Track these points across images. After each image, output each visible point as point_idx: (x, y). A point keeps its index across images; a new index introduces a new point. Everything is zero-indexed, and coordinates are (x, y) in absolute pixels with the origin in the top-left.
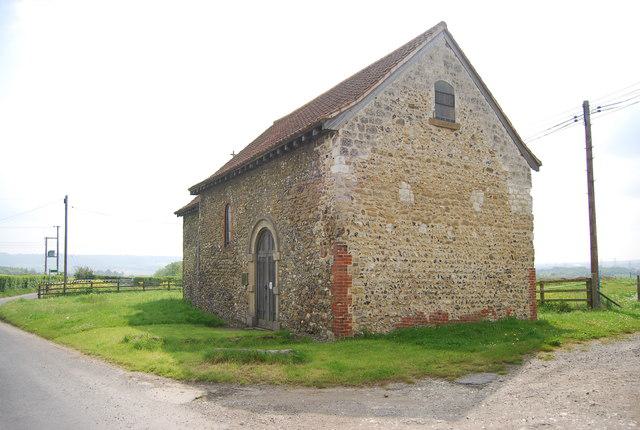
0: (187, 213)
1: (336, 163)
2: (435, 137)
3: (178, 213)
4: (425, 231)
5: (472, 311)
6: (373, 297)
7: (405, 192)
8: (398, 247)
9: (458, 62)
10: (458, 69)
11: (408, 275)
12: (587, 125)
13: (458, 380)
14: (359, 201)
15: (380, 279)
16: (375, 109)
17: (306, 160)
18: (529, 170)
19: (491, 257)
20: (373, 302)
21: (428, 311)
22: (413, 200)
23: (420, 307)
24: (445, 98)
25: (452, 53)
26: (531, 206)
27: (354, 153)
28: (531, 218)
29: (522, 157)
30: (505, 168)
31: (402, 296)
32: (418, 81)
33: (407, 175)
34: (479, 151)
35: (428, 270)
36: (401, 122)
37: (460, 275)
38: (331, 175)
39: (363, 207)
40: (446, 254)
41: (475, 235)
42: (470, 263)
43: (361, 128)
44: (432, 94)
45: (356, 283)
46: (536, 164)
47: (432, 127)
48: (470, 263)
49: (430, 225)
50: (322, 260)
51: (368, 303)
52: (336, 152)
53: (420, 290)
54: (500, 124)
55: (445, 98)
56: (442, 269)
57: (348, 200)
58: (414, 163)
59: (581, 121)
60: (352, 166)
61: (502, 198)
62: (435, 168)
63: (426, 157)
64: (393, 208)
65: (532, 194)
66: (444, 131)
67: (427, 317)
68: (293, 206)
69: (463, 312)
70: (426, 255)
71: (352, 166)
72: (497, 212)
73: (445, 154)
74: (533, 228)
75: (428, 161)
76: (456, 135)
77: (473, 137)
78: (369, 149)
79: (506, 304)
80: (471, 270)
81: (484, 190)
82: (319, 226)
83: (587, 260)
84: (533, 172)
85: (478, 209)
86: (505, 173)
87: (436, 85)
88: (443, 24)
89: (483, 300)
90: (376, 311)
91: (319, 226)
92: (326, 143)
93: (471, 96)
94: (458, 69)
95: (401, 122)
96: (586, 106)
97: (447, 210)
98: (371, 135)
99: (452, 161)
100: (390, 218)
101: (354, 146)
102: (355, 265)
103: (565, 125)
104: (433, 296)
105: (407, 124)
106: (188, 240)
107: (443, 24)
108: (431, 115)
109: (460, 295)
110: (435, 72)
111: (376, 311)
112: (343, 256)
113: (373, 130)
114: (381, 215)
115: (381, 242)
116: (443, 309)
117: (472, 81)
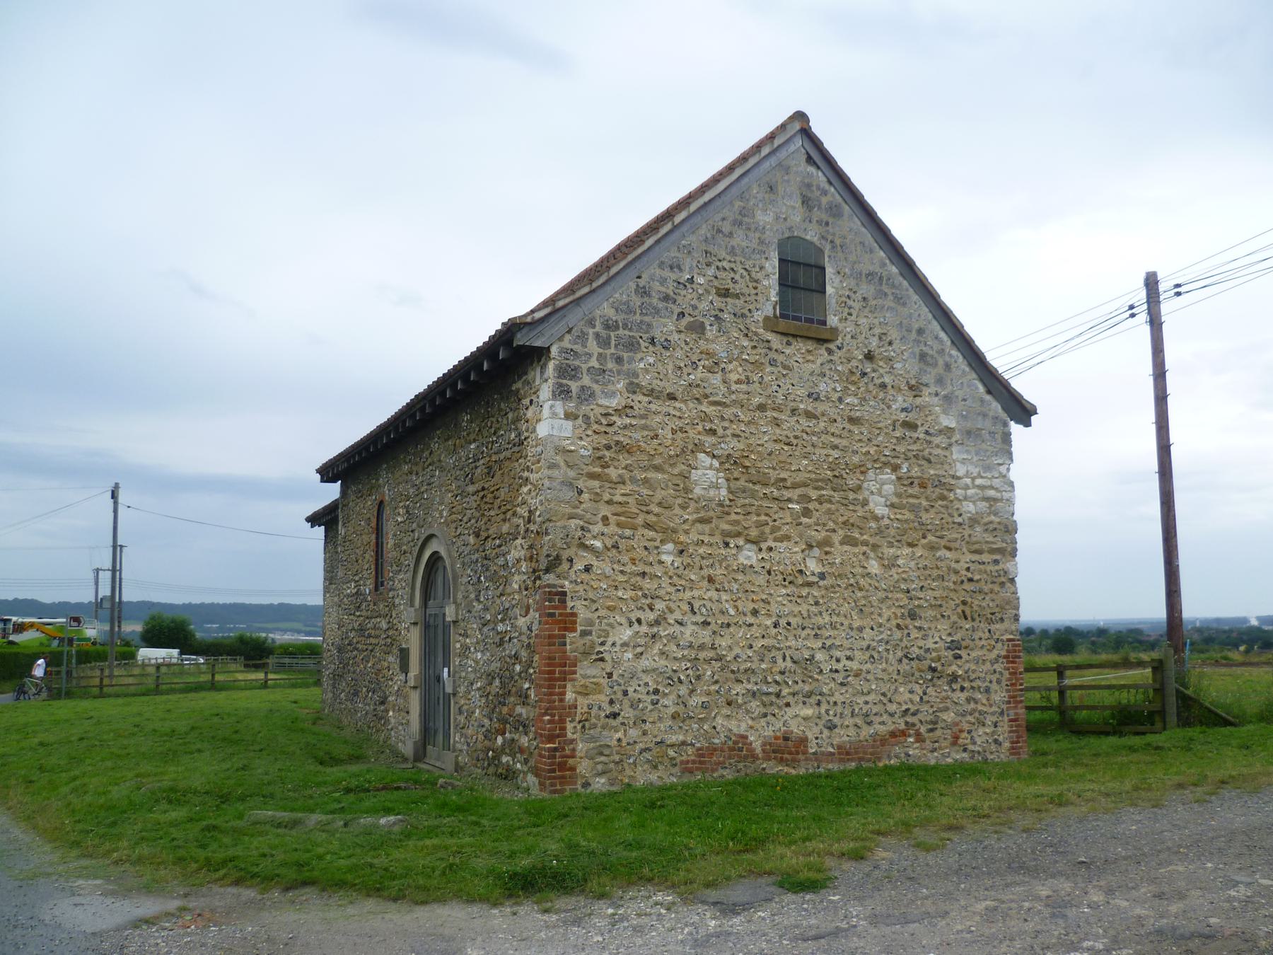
0: (325, 518)
1: (549, 421)
2: (780, 358)
3: (314, 520)
4: (754, 561)
5: (866, 732)
6: (626, 703)
7: (707, 476)
8: (688, 594)
9: (834, 195)
10: (834, 211)
11: (711, 654)
12: (1155, 323)
13: (713, 895)
14: (597, 498)
15: (645, 663)
16: (637, 301)
17: (500, 410)
18: (1006, 425)
19: (913, 616)
20: (628, 713)
21: (759, 734)
22: (724, 492)
23: (740, 725)
24: (801, 276)
25: (820, 178)
26: (1010, 502)
27: (586, 395)
28: (1010, 529)
29: (988, 397)
30: (948, 421)
31: (695, 700)
32: (739, 240)
33: (709, 440)
34: (883, 386)
35: (758, 644)
36: (698, 328)
37: (838, 654)
38: (539, 442)
39: (605, 511)
40: (804, 608)
41: (874, 567)
42: (861, 629)
43: (604, 342)
44: (772, 265)
45: (587, 671)
46: (1023, 412)
47: (770, 336)
48: (861, 629)
49: (764, 546)
50: (521, 622)
51: (615, 715)
52: (545, 392)
53: (738, 688)
54: (935, 326)
55: (801, 276)
56: (793, 643)
57: (569, 494)
58: (728, 413)
59: (1143, 317)
60: (580, 421)
61: (942, 488)
62: (777, 423)
63: (756, 400)
64: (677, 511)
65: (1013, 475)
66: (801, 346)
67: (757, 746)
68: (478, 508)
69: (843, 736)
70: (755, 613)
71: (580, 421)
72: (925, 517)
73: (802, 392)
74: (1016, 550)
75: (762, 407)
76: (830, 352)
77: (869, 357)
78: (620, 386)
79: (949, 717)
80: (865, 644)
81: (896, 468)
82: (517, 551)
83: (1156, 611)
84: (1015, 428)
85: (881, 510)
86: (948, 431)
87: (782, 245)
88: (800, 116)
89: (892, 707)
90: (634, 733)
91: (517, 551)
92: (530, 376)
93: (866, 267)
94: (834, 211)
95: (698, 328)
96: (1151, 283)
97: (807, 512)
98: (625, 355)
99: (821, 407)
100: (668, 533)
101: (586, 380)
102: (585, 633)
103: (1108, 324)
104: (772, 701)
105: (711, 332)
106: (331, 577)
107: (800, 116)
108: (768, 310)
109: (838, 697)
110: (779, 216)
111: (634, 733)
112: (559, 616)
113: (632, 346)
114: (648, 526)
115: (647, 584)
116: (796, 728)
117: (867, 236)
